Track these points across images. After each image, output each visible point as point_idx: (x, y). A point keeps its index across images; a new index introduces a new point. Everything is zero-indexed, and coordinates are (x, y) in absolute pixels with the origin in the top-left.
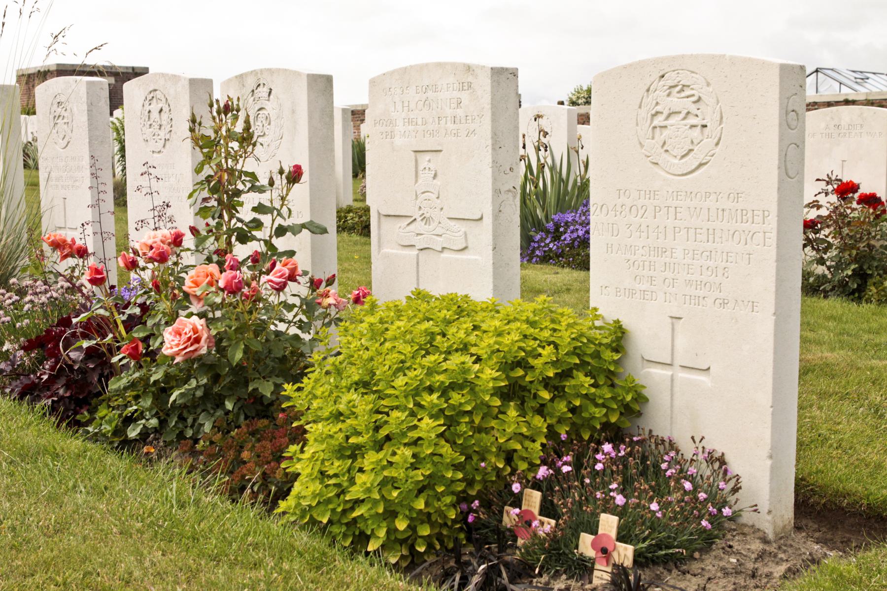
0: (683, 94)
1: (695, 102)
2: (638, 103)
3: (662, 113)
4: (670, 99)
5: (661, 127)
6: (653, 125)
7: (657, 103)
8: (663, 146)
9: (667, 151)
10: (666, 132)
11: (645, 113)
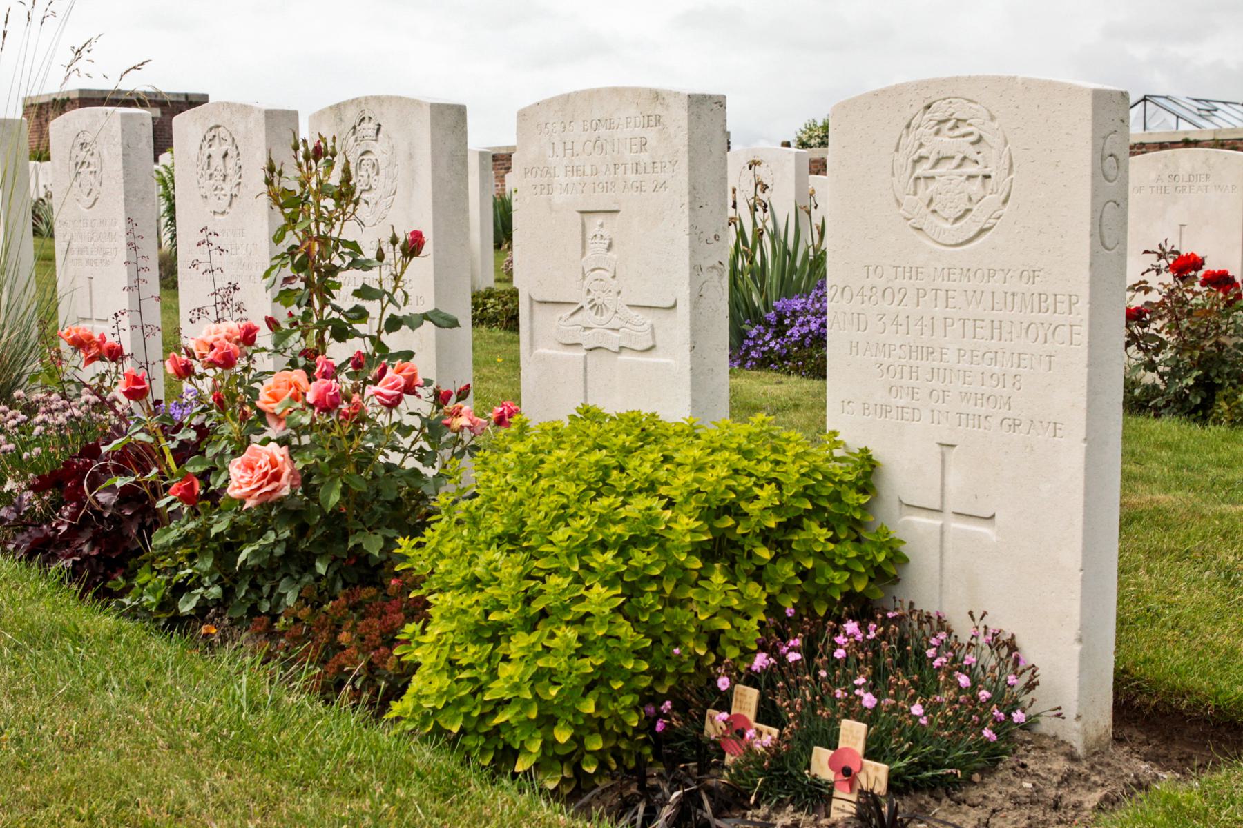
1: (973, 143)
3: (927, 158)
5: (926, 178)
6: (915, 175)
7: (921, 145)
8: (928, 205)
9: (934, 211)
10: (933, 186)
11: (903, 159)
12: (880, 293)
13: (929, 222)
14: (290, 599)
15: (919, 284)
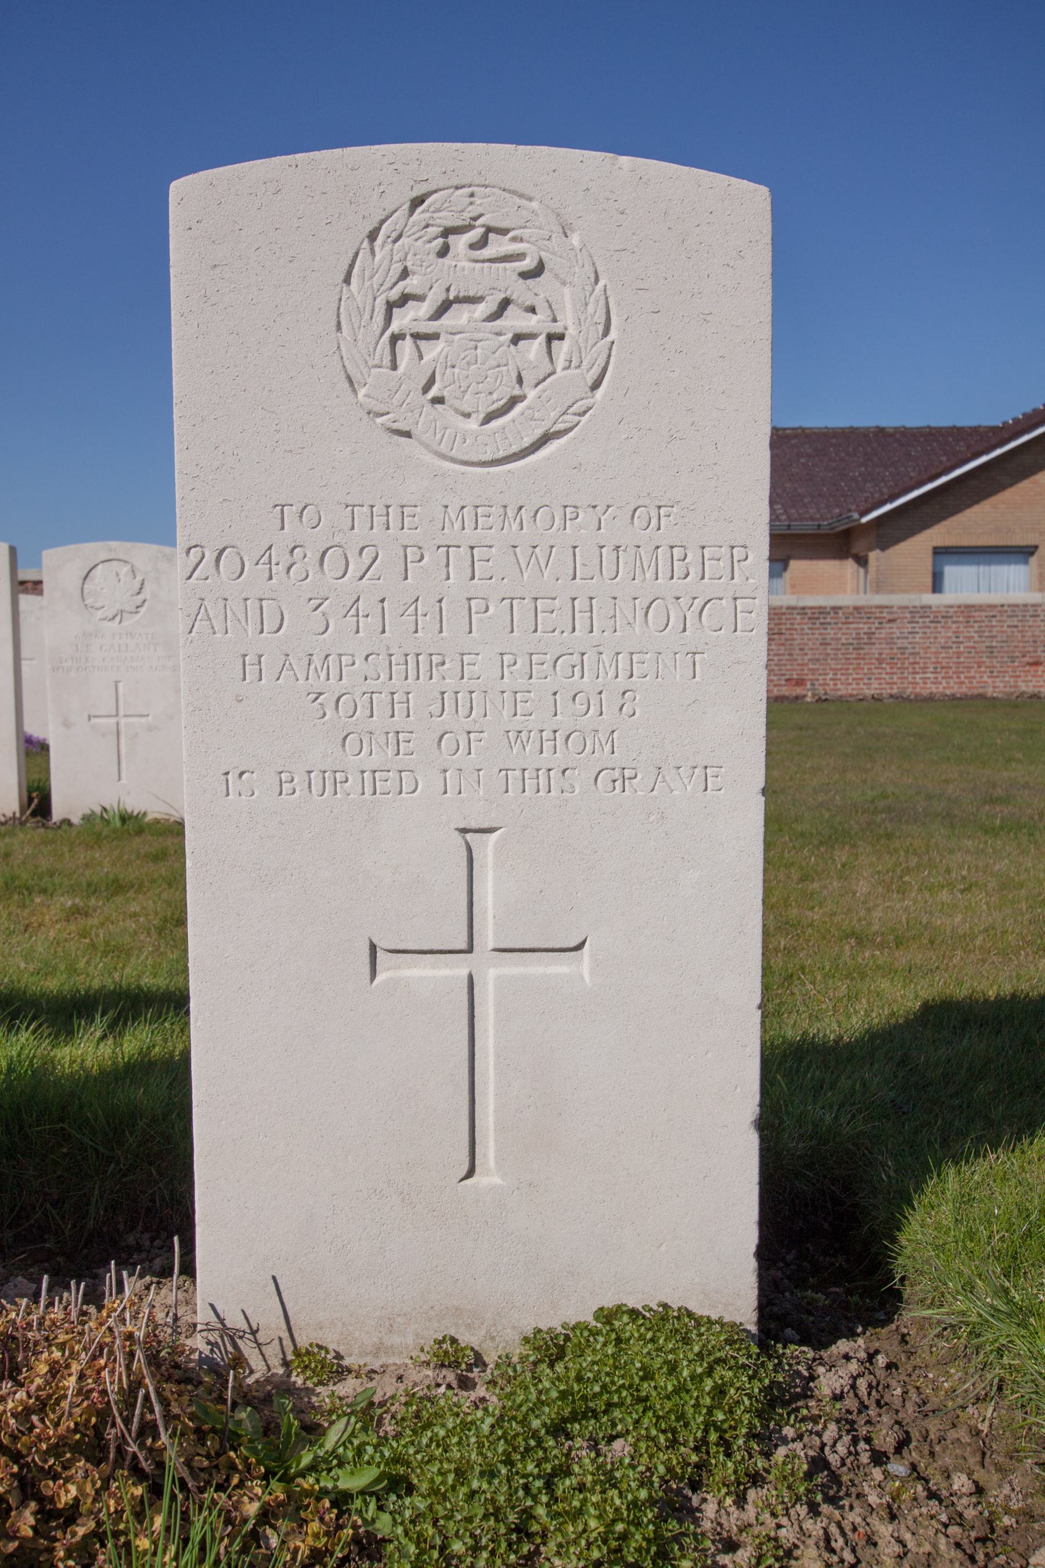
0: (487, 252)
1: (525, 275)
2: (334, 323)
3: (421, 298)
4: (447, 261)
5: (417, 337)
6: (395, 327)
7: (405, 274)
8: (426, 389)
9: (439, 400)
10: (433, 351)
11: (366, 294)
12: (313, 556)
13: (425, 420)
14: (999, 741)
15: (408, 536)
